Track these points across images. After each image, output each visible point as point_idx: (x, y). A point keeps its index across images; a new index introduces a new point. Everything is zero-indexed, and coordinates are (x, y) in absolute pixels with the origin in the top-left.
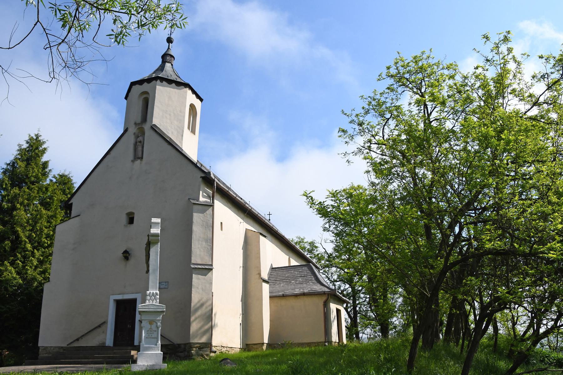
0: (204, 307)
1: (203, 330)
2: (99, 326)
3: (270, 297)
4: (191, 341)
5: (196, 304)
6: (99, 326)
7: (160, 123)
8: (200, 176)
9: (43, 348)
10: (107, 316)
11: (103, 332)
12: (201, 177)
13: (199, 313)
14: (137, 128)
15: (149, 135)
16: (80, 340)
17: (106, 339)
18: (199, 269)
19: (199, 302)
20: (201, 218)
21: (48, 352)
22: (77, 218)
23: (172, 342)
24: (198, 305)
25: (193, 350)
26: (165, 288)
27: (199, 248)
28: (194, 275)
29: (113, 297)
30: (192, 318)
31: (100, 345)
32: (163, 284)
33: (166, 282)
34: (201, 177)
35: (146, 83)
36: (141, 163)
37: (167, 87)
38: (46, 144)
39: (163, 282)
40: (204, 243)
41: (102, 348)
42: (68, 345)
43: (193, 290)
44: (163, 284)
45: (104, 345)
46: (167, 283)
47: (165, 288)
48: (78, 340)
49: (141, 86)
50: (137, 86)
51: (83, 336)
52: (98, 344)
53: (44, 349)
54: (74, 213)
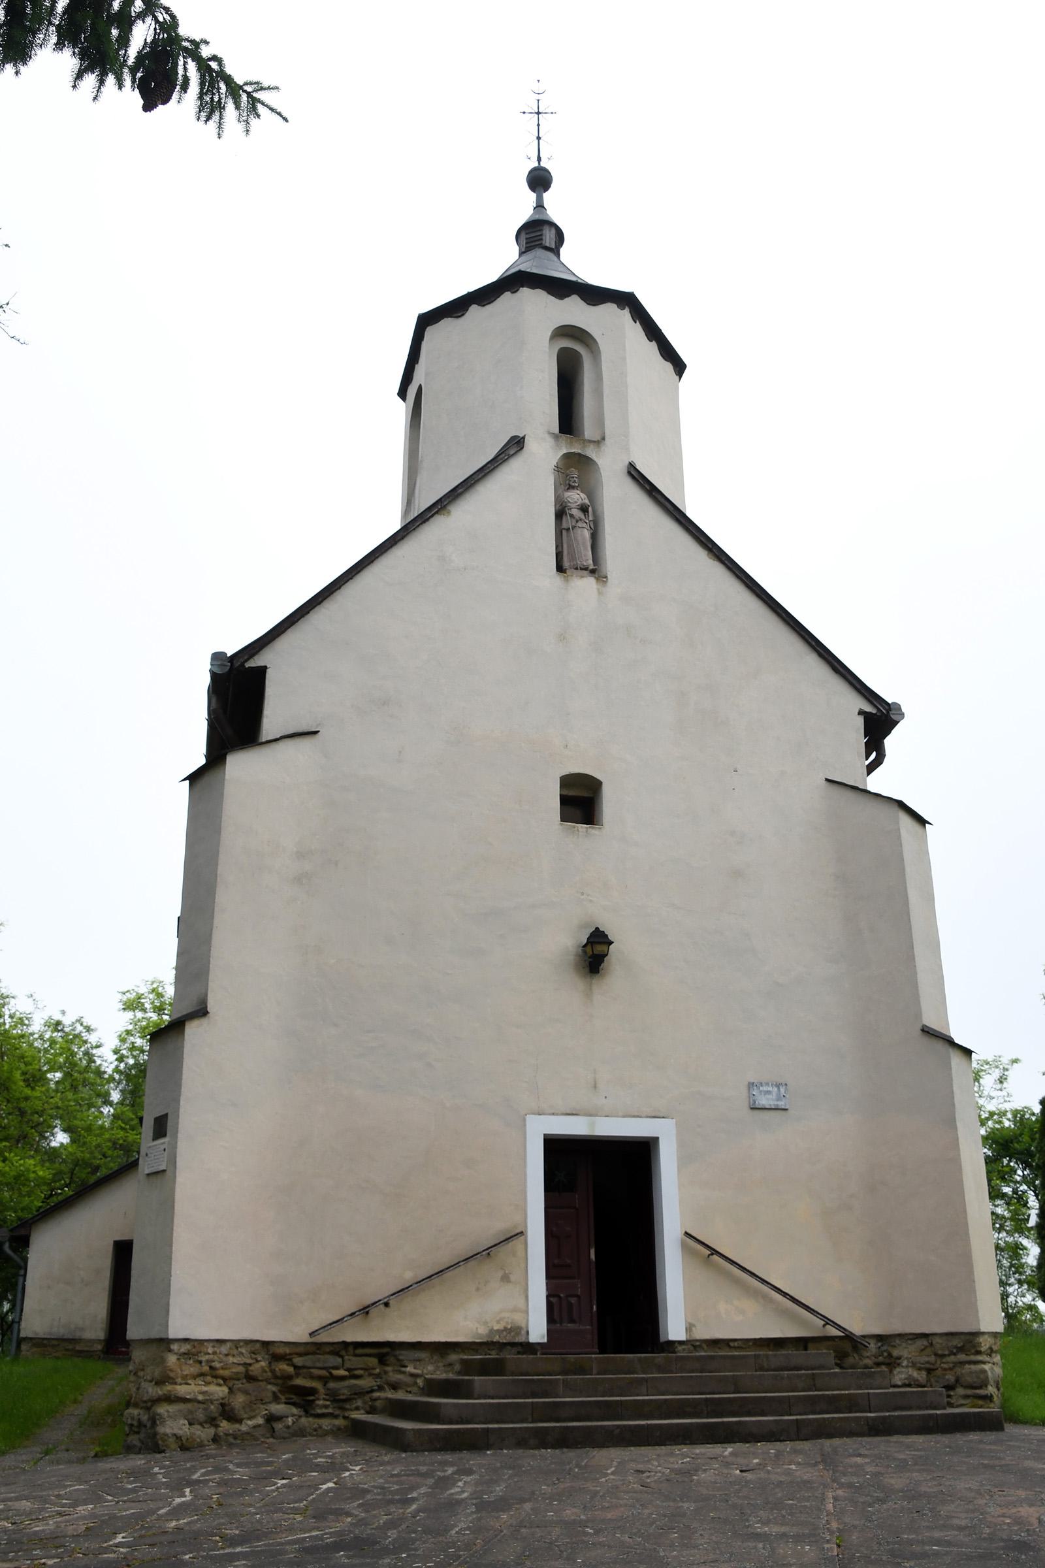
9: (185, 1348)
11: (506, 1278)
12: (861, 712)
14: (565, 451)
17: (527, 1312)
23: (839, 1327)
29: (539, 1128)
31: (496, 1338)
32: (769, 1092)
34: (861, 712)
36: (600, 593)
39: (767, 1084)
44: (769, 1092)
45: (521, 1339)
46: (782, 1090)
48: (365, 1311)
54: (273, 721)
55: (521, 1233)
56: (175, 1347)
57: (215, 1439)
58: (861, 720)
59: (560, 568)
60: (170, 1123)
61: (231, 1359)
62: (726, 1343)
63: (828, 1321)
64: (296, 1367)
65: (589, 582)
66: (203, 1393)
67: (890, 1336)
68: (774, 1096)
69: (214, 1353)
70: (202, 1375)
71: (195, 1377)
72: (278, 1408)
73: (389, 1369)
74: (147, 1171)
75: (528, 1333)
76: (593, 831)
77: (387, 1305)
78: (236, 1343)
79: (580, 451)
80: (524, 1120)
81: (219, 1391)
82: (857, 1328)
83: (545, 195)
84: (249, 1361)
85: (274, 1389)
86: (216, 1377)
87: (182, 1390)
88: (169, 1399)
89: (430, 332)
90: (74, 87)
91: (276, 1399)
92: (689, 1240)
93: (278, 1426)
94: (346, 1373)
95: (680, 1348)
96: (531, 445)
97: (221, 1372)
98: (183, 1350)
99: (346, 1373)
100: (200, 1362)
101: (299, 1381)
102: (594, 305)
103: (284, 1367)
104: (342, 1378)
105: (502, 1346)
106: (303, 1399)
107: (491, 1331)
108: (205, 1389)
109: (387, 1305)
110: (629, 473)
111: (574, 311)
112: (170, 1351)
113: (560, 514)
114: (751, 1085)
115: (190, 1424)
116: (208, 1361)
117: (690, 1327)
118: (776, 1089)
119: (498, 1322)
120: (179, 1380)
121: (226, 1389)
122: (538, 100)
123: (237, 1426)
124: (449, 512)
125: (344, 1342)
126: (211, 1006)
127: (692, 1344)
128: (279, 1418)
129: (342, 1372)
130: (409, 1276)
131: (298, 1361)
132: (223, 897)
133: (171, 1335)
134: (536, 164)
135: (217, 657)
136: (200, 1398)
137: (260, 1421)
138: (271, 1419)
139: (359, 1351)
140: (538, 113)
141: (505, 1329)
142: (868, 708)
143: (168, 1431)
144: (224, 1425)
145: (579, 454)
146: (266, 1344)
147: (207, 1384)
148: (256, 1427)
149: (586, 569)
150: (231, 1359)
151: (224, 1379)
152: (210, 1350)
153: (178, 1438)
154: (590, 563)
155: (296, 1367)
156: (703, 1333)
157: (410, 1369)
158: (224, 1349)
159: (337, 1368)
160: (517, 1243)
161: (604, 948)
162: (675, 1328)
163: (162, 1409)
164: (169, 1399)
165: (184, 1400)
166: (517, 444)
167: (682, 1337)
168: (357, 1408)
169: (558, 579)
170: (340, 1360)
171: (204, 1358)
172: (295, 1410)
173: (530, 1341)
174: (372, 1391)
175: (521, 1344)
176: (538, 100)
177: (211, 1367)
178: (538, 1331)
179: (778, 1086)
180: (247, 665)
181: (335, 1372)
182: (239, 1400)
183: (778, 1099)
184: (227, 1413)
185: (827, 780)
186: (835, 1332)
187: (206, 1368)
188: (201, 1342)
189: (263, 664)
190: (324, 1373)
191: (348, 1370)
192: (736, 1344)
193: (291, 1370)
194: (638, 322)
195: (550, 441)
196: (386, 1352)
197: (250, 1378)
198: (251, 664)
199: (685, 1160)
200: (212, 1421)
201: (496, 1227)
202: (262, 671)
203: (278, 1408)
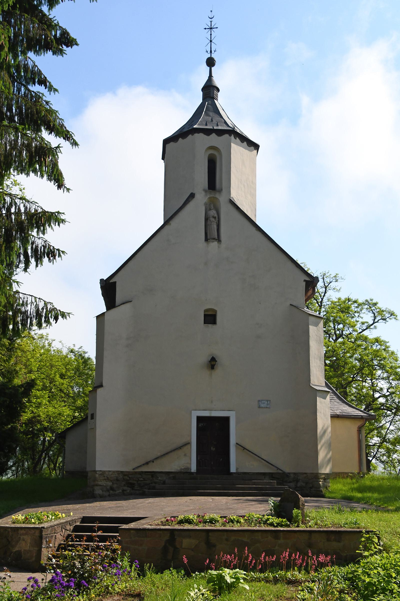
0: (326, 435)
1: (327, 459)
2: (180, 448)
3: (331, 417)
4: (320, 472)
5: (321, 432)
6: (180, 448)
7: (237, 196)
8: (303, 280)
9: (101, 473)
10: (190, 436)
11: (185, 455)
12: (305, 281)
13: (323, 441)
14: (209, 196)
15: (166, 220)
16: (151, 464)
17: (191, 464)
18: (320, 391)
19: (323, 428)
20: (315, 332)
21: (106, 478)
22: (128, 305)
23: (282, 471)
24: (322, 432)
25: (320, 481)
26: (267, 408)
27: (315, 366)
28: (317, 397)
29: (195, 414)
30: (319, 447)
31: (183, 471)
32: (264, 403)
33: (267, 401)
34: (305, 281)
35: (214, 135)
36: (219, 247)
37: (246, 149)
38: (234, 139)
39: (264, 401)
40: (318, 361)
41: (186, 473)
42: (133, 469)
43: (318, 414)
44: (264, 403)
45: (189, 471)
46: (269, 402)
47: (267, 408)
48: (147, 463)
49: (176, 143)
50: (172, 144)
51: (157, 458)
52: (179, 469)
53: (101, 474)
54: (118, 299)
55: (189, 443)
56: (98, 472)
57: (109, 495)
58: (304, 283)
59: (207, 240)
60: (94, 416)
61: (112, 476)
62: (248, 473)
63: (278, 469)
64: (129, 478)
65: (215, 243)
66: (105, 484)
67: (297, 473)
68: (266, 404)
69: (108, 474)
70: (105, 479)
71: (103, 480)
72: (125, 488)
73: (154, 478)
74: (90, 428)
75: (191, 469)
76: (214, 326)
77: (153, 462)
78: (114, 472)
79: (213, 196)
80: (191, 412)
81: (110, 484)
82: (287, 470)
83: (212, 68)
84: (117, 476)
85: (124, 483)
86: (109, 480)
87: (100, 483)
88: (97, 485)
89: (167, 146)
90: (50, 94)
91: (124, 485)
92: (238, 446)
93: (125, 492)
94: (143, 479)
95: (234, 474)
96: (197, 196)
97: (110, 479)
98: (100, 473)
99: (143, 479)
100: (104, 476)
101: (131, 481)
102: (220, 136)
103: (126, 477)
104: (142, 481)
105: (184, 473)
106: (131, 485)
107: (181, 469)
108: (106, 483)
109: (153, 462)
110: (230, 202)
111: (213, 139)
112: (97, 473)
113: (206, 219)
114: (259, 401)
115: (103, 491)
116: (107, 476)
117: (237, 469)
118: (267, 402)
119: (183, 466)
120: (99, 481)
121: (111, 483)
122: (211, 22)
123: (115, 492)
124: (170, 224)
125: (142, 471)
126: (104, 384)
127: (237, 473)
128: (126, 490)
129: (142, 479)
130: (159, 454)
131: (130, 476)
132: (106, 353)
133: (97, 469)
134: (210, 56)
135: (102, 280)
136: (105, 485)
137: (121, 491)
138: (123, 491)
139: (146, 474)
140: (211, 28)
141: (185, 468)
142: (308, 279)
143: (97, 493)
144: (111, 492)
145: (214, 197)
146: (122, 472)
147: (107, 482)
148: (119, 492)
149: (214, 239)
150: (112, 476)
151: (111, 481)
152: (107, 473)
153: (99, 495)
154: (216, 237)
155: (129, 478)
156: (241, 470)
157: (159, 478)
158: (111, 473)
159: (140, 478)
160: (188, 446)
161: (215, 363)
162: (233, 469)
163: (96, 488)
164: (97, 485)
165: (101, 485)
166: (192, 196)
167: (235, 472)
168: (146, 488)
169: (205, 244)
170: (141, 476)
171: (105, 475)
172: (129, 489)
173: (192, 471)
174: (149, 484)
175: (189, 472)
176: (211, 22)
177: (107, 478)
178: (194, 469)
179: (267, 401)
180: (110, 282)
181: (140, 479)
182: (115, 486)
183: (267, 405)
184: (112, 489)
185: (291, 305)
186: (281, 472)
187: (106, 478)
188: (105, 471)
189: (115, 281)
190: (137, 479)
191: (143, 478)
192: (251, 474)
193: (128, 478)
194: (237, 138)
195: (203, 193)
196: (153, 474)
197: (117, 480)
198: (111, 281)
199: (237, 423)
200: (108, 490)
201: (184, 441)
202: (115, 283)
203: (125, 488)
